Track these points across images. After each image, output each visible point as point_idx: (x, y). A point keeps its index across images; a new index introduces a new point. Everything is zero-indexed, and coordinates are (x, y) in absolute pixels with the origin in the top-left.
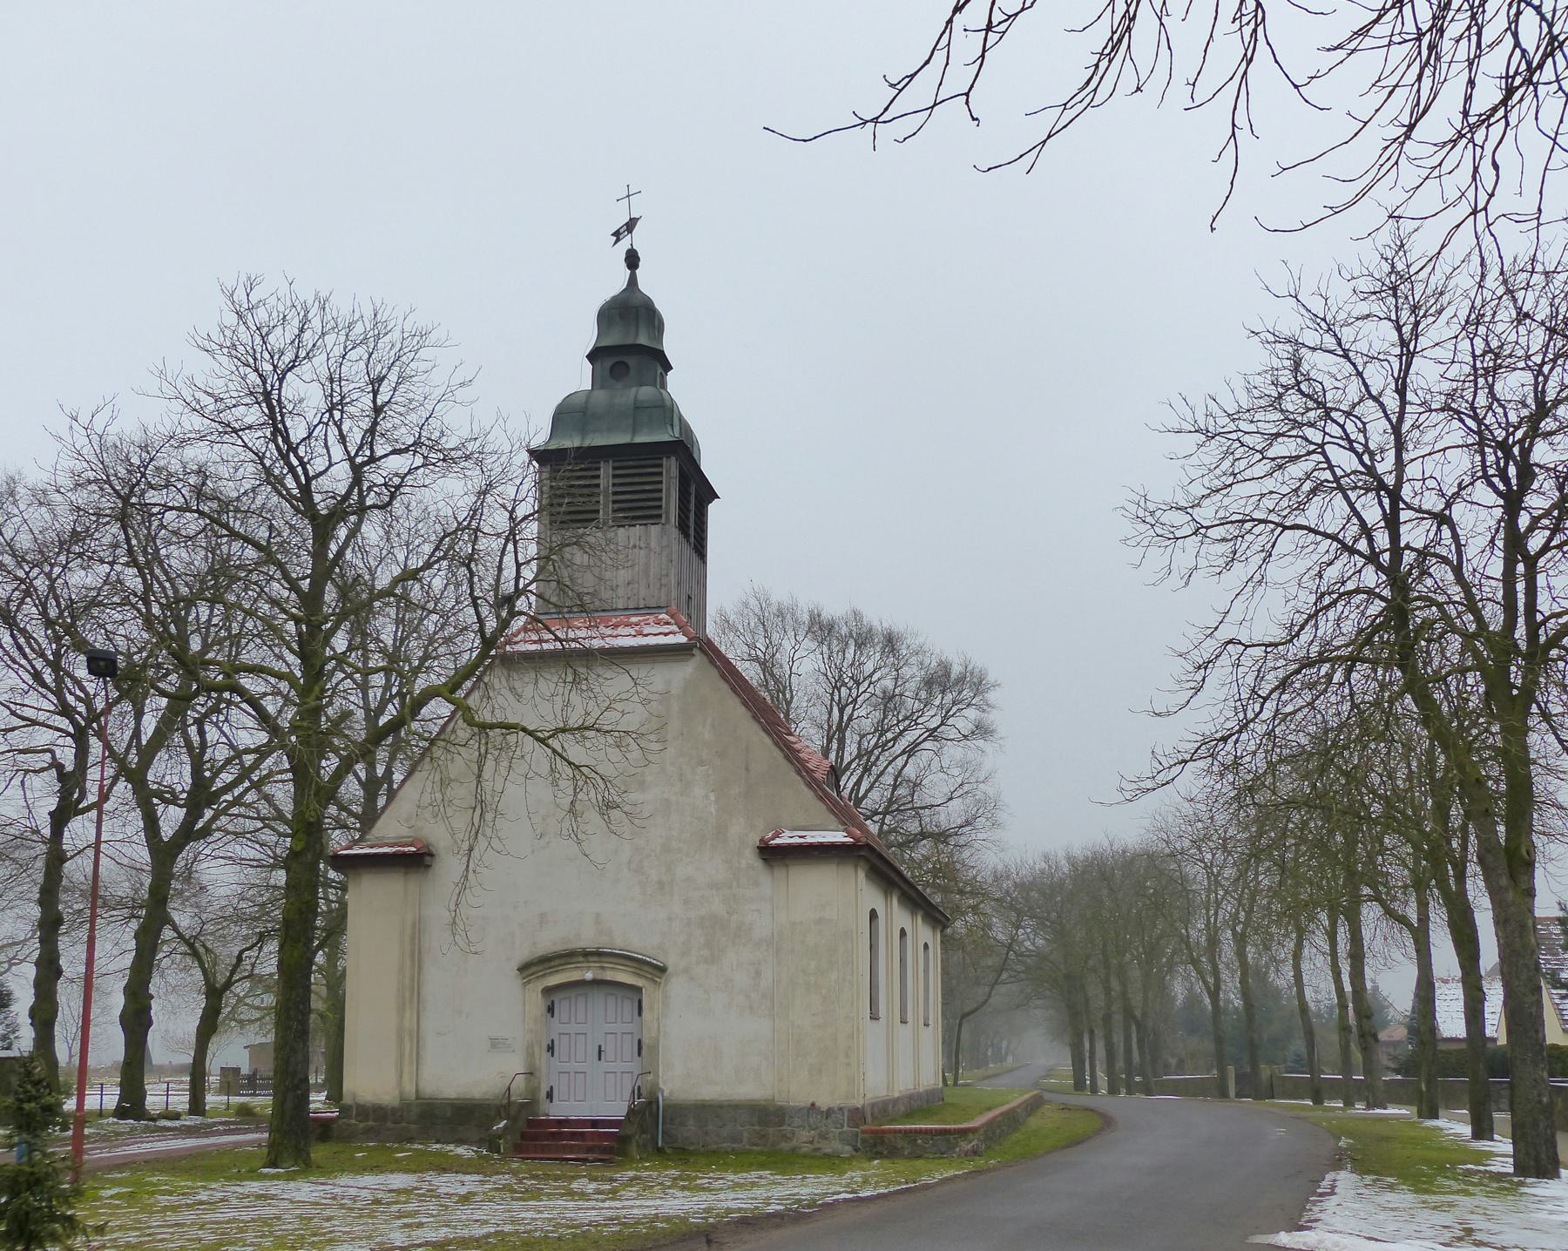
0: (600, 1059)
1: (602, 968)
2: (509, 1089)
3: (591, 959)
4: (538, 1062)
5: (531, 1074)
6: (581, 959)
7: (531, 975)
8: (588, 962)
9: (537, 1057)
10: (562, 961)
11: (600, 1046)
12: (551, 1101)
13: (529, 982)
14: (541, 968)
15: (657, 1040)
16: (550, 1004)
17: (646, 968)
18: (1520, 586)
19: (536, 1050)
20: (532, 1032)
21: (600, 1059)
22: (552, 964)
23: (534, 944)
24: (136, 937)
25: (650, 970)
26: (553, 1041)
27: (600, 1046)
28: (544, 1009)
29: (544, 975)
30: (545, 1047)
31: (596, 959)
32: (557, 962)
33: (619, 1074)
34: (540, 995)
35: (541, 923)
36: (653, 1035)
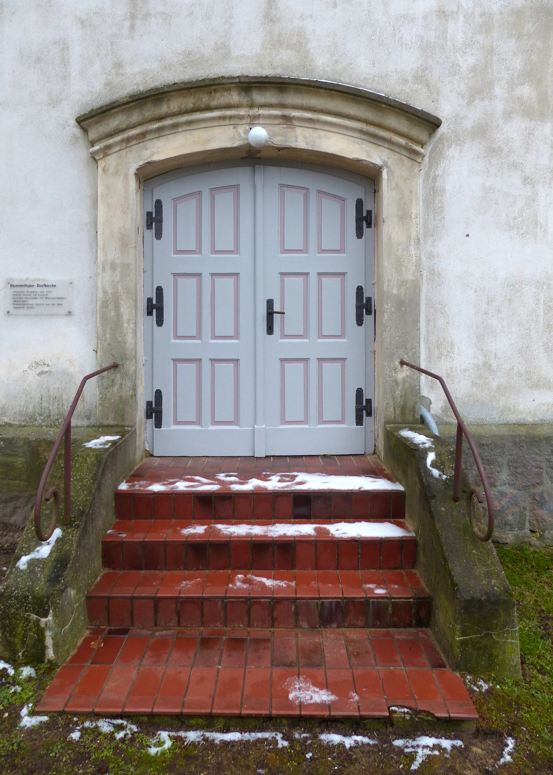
0: (270, 330)
1: (287, 119)
2: (68, 429)
3: (258, 97)
4: (130, 338)
5: (115, 366)
6: (235, 97)
7: (111, 135)
8: (251, 106)
9: (128, 327)
10: (189, 102)
11: (270, 303)
12: (158, 424)
13: (106, 151)
14: (135, 117)
15: (416, 287)
16: (151, 208)
17: (392, 121)
18: (402, 141)
19: (126, 310)
20: (113, 266)
21: (270, 330)
22: (164, 109)
23: (118, 65)
24: (420, 434)
25: (401, 124)
26: (159, 291)
27: (270, 303)
28: (141, 221)
29: (143, 135)
30: (142, 305)
31: (270, 97)
32: (175, 105)
33: (313, 365)
34: (133, 183)
35: (133, 17)
36: (410, 276)
